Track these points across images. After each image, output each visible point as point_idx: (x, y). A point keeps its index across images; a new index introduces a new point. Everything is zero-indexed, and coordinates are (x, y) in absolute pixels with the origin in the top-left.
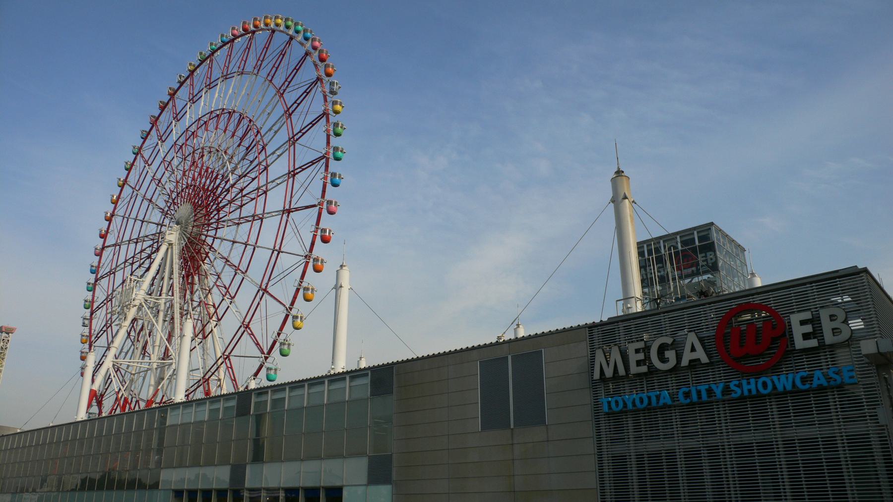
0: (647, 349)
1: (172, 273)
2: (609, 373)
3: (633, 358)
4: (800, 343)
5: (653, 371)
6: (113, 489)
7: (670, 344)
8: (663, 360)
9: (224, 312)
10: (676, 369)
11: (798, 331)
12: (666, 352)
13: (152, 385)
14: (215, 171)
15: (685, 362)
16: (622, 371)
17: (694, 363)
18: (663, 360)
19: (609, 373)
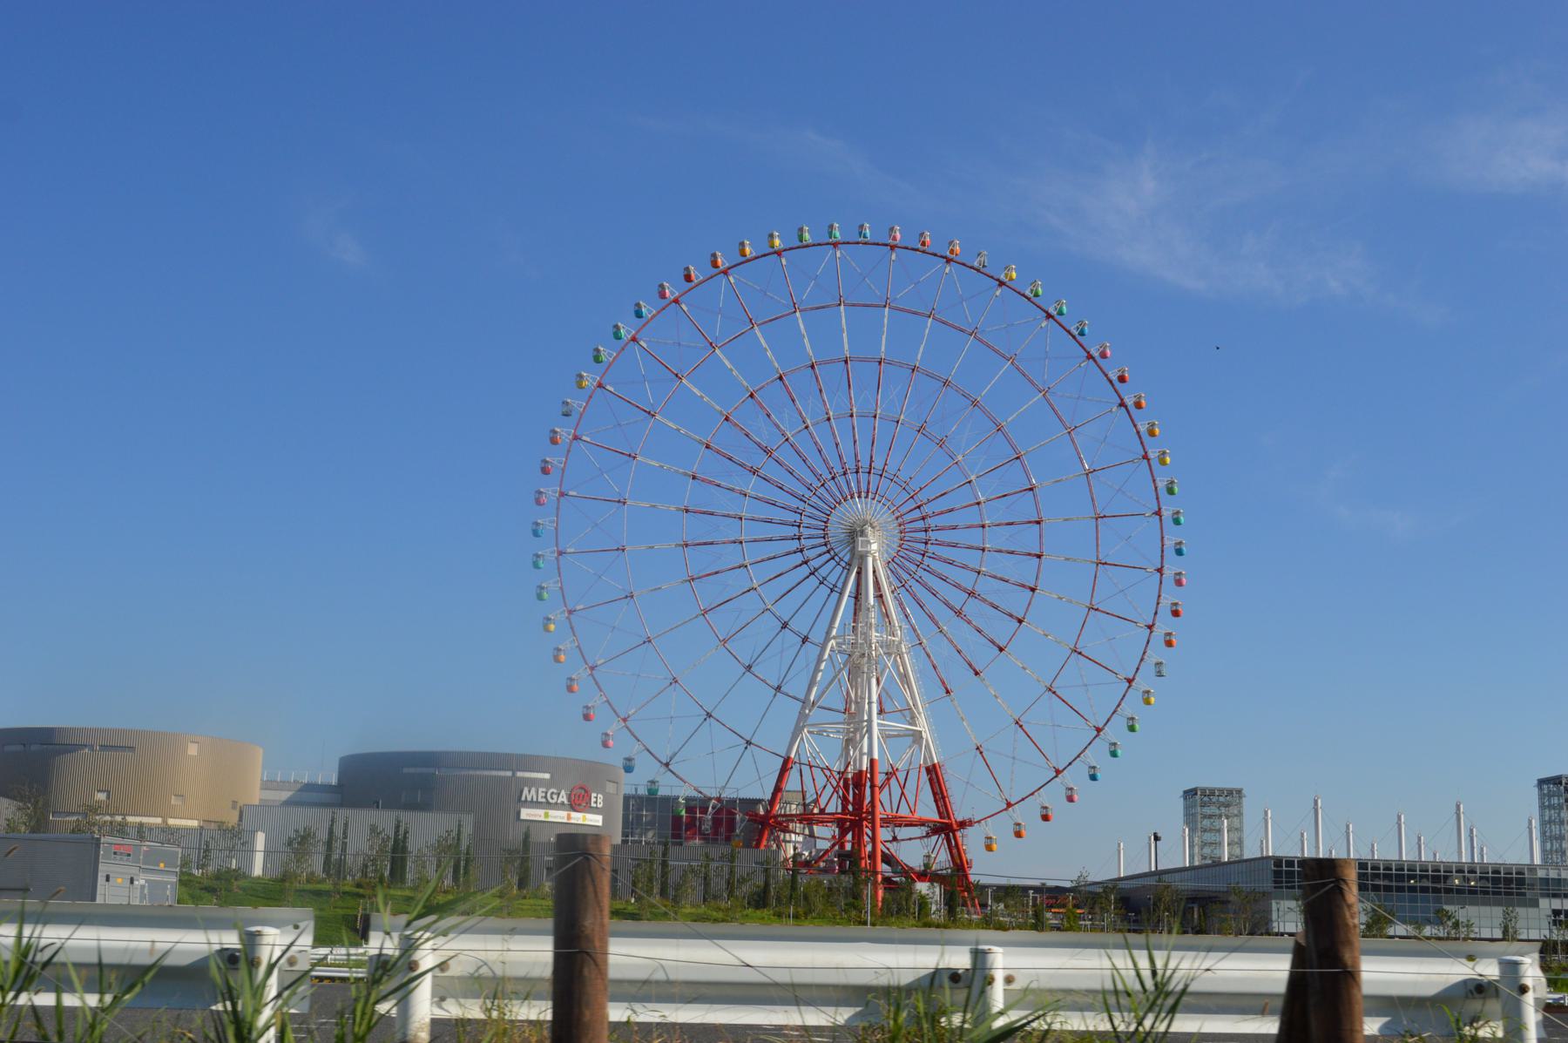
0: (546, 793)
1: (880, 597)
2: (529, 799)
3: (541, 794)
4: (593, 805)
5: (548, 802)
6: (1359, 869)
7: (607, 791)
8: (552, 799)
9: (834, 606)
10: (556, 803)
11: (593, 800)
12: (334, 781)
13: (865, 754)
14: (787, 835)
15: (559, 802)
16: (535, 799)
17: (563, 803)
18: (552, 799)
19: (529, 799)
